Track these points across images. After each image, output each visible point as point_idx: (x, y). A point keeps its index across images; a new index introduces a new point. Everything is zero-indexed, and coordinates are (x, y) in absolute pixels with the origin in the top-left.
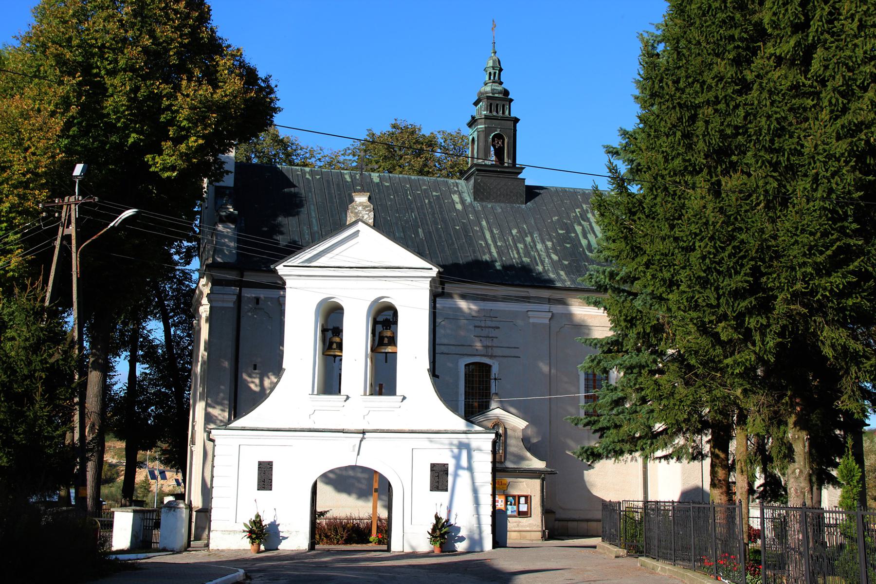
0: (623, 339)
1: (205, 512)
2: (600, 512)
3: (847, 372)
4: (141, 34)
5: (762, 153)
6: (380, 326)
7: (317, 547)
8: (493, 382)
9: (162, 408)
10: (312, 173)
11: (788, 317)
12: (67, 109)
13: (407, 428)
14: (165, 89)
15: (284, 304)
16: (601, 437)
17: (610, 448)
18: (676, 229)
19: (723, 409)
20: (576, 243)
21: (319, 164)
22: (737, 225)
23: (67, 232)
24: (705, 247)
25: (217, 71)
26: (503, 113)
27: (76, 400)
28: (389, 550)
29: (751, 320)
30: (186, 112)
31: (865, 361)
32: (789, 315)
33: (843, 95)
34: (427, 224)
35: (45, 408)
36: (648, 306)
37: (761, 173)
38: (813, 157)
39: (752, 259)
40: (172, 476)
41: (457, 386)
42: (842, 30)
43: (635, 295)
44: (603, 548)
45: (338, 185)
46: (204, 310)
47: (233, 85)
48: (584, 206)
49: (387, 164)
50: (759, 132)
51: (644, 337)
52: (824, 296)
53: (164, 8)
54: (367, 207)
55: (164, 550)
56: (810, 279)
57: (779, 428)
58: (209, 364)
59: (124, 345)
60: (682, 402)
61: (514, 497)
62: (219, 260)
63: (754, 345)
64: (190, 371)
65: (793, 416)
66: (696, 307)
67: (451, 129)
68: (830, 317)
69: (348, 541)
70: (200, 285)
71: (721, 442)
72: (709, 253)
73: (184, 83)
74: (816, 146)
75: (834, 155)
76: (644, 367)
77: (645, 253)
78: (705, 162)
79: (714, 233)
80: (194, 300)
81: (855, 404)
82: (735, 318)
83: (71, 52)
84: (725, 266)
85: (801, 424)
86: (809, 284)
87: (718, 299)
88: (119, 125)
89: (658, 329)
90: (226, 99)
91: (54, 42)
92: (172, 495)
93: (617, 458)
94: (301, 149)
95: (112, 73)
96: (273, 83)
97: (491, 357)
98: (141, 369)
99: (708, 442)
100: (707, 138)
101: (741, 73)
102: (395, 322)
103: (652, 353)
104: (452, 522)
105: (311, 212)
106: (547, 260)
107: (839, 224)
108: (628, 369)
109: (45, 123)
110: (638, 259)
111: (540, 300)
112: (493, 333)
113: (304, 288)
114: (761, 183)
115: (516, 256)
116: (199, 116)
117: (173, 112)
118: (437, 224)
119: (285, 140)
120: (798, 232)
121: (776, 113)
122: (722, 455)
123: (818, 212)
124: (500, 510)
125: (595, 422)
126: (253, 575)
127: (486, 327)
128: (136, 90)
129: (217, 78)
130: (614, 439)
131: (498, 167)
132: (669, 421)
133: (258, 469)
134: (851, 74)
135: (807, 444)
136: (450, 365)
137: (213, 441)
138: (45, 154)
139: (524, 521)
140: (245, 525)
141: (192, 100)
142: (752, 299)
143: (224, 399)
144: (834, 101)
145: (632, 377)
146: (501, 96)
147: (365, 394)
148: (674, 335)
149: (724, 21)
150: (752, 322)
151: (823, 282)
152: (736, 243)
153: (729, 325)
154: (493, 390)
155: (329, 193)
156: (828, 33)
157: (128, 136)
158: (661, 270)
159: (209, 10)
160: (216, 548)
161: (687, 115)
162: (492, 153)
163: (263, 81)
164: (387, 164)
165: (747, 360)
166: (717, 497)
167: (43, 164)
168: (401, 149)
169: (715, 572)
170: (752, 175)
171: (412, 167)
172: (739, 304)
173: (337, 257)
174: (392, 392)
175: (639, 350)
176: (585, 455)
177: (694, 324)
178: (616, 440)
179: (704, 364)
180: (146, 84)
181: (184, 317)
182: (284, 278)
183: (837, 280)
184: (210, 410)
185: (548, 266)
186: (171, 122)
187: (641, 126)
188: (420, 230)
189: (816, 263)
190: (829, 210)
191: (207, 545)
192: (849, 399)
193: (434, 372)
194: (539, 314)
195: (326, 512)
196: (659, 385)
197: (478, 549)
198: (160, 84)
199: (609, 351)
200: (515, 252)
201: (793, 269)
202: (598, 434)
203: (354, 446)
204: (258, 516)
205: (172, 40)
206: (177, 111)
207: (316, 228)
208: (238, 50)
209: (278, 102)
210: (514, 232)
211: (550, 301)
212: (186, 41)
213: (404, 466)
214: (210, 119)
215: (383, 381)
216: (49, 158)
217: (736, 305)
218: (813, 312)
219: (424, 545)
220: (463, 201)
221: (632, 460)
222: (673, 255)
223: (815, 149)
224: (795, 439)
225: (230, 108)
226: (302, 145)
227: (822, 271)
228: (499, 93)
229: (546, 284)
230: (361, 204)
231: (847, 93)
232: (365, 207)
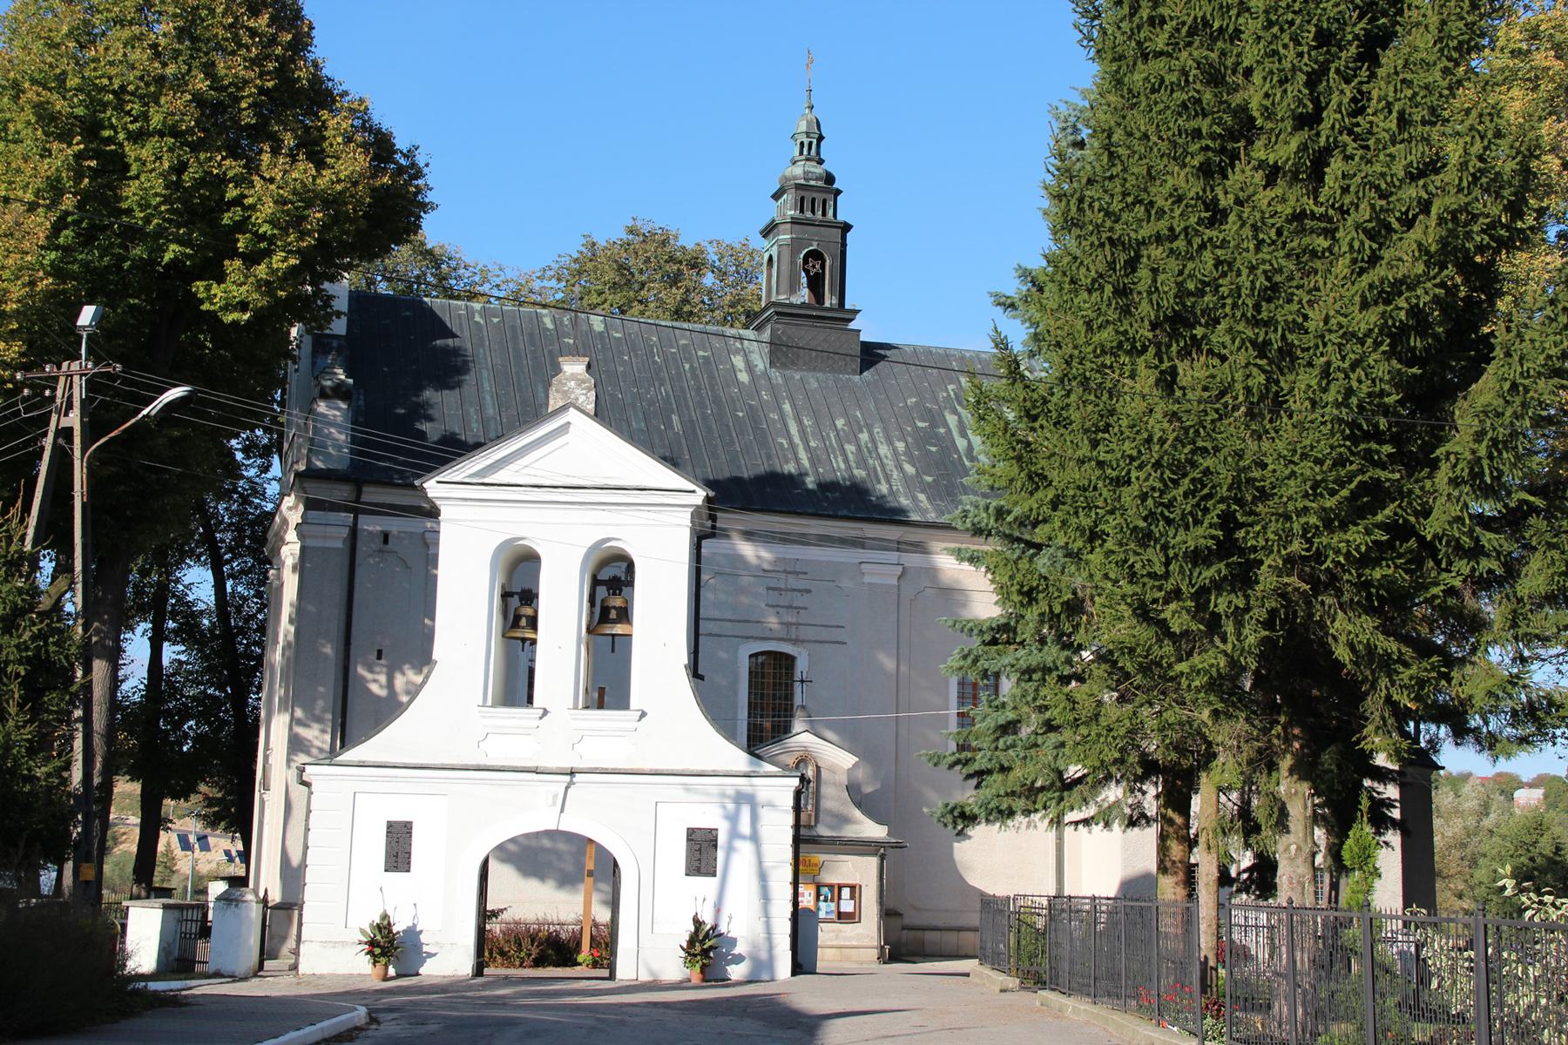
1: (290, 906)
2: (978, 915)
3: (1374, 687)
4: (189, 70)
6: (604, 588)
8: (797, 685)
9: (208, 722)
10: (485, 313)
11: (1280, 595)
12: (55, 203)
13: (647, 766)
14: (231, 168)
15: (437, 544)
16: (978, 786)
18: (1101, 448)
20: (948, 446)
22: (1200, 444)
23: (65, 422)
24: (1147, 479)
25: (324, 138)
26: (824, 214)
27: (78, 713)
28: (612, 977)
30: (268, 208)
31: (1401, 669)
34: (688, 408)
35: (24, 727)
36: (1058, 566)
37: (1241, 358)
38: (1322, 337)
39: (1222, 500)
40: (223, 843)
41: (735, 693)
42: (1370, 132)
45: (531, 335)
46: (290, 551)
47: (351, 163)
49: (618, 298)
51: (1051, 619)
53: (231, 26)
54: (584, 382)
57: (1269, 774)
58: (301, 646)
59: (142, 611)
60: (1111, 730)
61: (831, 887)
62: (319, 464)
63: (1224, 641)
64: (260, 659)
65: (1288, 756)
67: (733, 237)
68: (1346, 597)
69: (539, 962)
70: (284, 507)
71: (1176, 799)
72: (1153, 489)
75: (1354, 335)
76: (1050, 670)
77: (1050, 484)
80: (270, 535)
83: (64, 98)
84: (1178, 511)
85: (1303, 769)
86: (1312, 543)
87: (1167, 564)
89: (1075, 607)
90: (339, 187)
91: (34, 81)
92: (223, 879)
94: (466, 268)
95: (138, 137)
96: (421, 160)
97: (795, 641)
98: (171, 653)
101: (1212, 190)
102: (631, 583)
104: (723, 929)
105: (482, 382)
106: (895, 474)
107: (1363, 446)
108: (1023, 673)
109: (18, 224)
110: (1040, 494)
111: (882, 545)
112: (800, 600)
113: (471, 520)
115: (842, 466)
117: (245, 208)
118: (705, 407)
119: (437, 251)
120: (1296, 459)
121: (1264, 262)
122: (1179, 820)
123: (1329, 426)
124: (807, 910)
125: (967, 762)
126: (381, 1016)
127: (786, 590)
128: (180, 168)
131: (814, 309)
132: (1089, 762)
133: (379, 836)
134: (1384, 202)
136: (722, 655)
137: (307, 784)
138: (18, 278)
139: (848, 929)
140: (363, 932)
142: (1222, 566)
144: (1356, 245)
146: (820, 184)
147: (576, 707)
149: (1184, 105)
150: (1221, 603)
151: (1336, 539)
152: (1196, 474)
154: (798, 700)
155: (515, 350)
156: (1350, 132)
157: (162, 250)
158: (1076, 513)
159: (311, 28)
161: (1123, 257)
162: (804, 280)
163: (405, 156)
164: (618, 298)
165: (1212, 666)
166: (1170, 888)
167: (14, 296)
168: (644, 277)
169: (1159, 1013)
170: (1222, 365)
171: (661, 303)
173: (526, 471)
174: (622, 703)
175: (1043, 641)
176: (949, 818)
179: (1145, 669)
181: (250, 561)
182: (438, 503)
183: (1357, 537)
184: (300, 730)
185: (898, 485)
188: (675, 418)
189: (1324, 509)
190: (1347, 424)
191: (295, 967)
193: (695, 671)
195: (502, 911)
196: (1074, 702)
197: (765, 977)
198: (224, 158)
199: (994, 642)
200: (840, 459)
201: (1288, 518)
202: (974, 782)
204: (385, 916)
205: (246, 82)
206: (253, 207)
207: (490, 411)
208: (362, 101)
211: (900, 546)
212: (270, 84)
213: (641, 834)
215: (607, 687)
216: (24, 285)
218: (1317, 587)
219: (672, 967)
220: (750, 368)
222: (1095, 489)
224: (1290, 796)
226: (468, 260)
228: (817, 179)
229: (892, 516)
230: (574, 377)
231: (1379, 232)
232: (580, 382)
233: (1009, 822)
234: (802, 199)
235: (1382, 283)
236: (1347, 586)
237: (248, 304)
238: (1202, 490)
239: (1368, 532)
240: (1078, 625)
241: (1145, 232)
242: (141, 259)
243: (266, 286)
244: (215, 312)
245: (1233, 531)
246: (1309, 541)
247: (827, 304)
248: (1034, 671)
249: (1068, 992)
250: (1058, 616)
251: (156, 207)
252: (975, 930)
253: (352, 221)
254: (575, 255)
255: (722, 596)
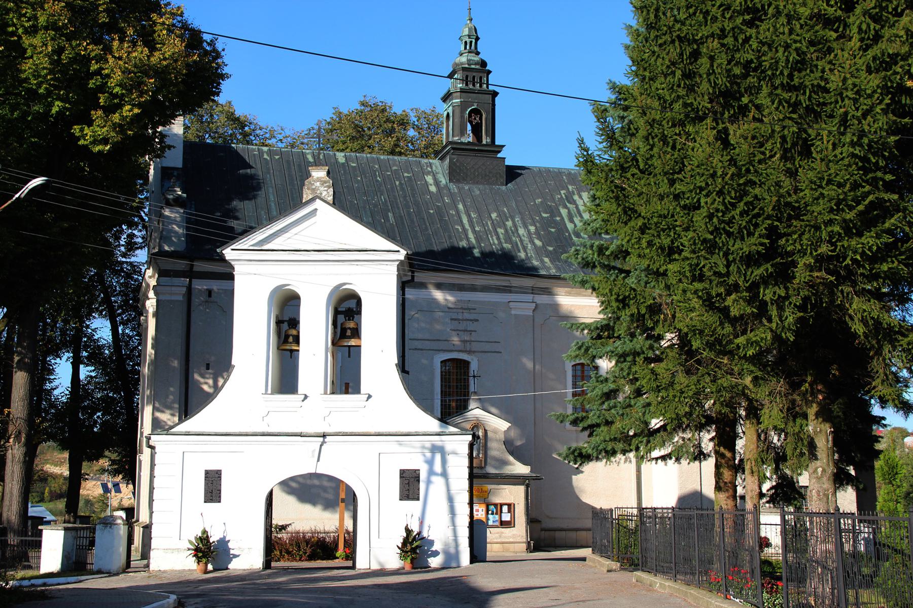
0: (615, 323)
5: (779, 91)
7: (273, 564)
8: (471, 378)
10: (270, 153)
13: (372, 431)
14: (93, 50)
16: (590, 435)
17: (600, 448)
19: (730, 401)
20: (562, 227)
21: (280, 145)
22: (750, 177)
24: (713, 203)
25: (155, 32)
26: (481, 86)
28: (353, 567)
29: (767, 291)
30: (118, 76)
31: (901, 338)
32: (811, 285)
33: (876, 19)
34: (398, 208)
36: (643, 284)
38: (841, 94)
39: (769, 217)
40: (126, 489)
41: (432, 384)
43: (628, 273)
44: (594, 561)
45: (299, 166)
46: (151, 304)
47: (172, 47)
48: (570, 187)
49: (356, 145)
50: (775, 65)
52: (854, 261)
54: (325, 182)
55: (99, 572)
56: (838, 240)
60: (682, 392)
61: (496, 505)
62: (167, 248)
63: (770, 320)
65: (814, 405)
66: (701, 278)
67: (425, 107)
69: (312, 558)
70: (146, 276)
71: (726, 440)
72: (717, 210)
73: (116, 44)
74: (845, 80)
76: (639, 354)
77: (640, 215)
78: (709, 106)
79: (724, 187)
80: (141, 294)
81: (890, 390)
82: (748, 289)
84: (736, 226)
85: (824, 414)
87: (728, 266)
88: (41, 91)
90: (165, 63)
93: (608, 459)
94: (261, 129)
95: (33, 31)
96: (219, 46)
97: (470, 352)
99: (711, 440)
100: (712, 78)
102: (359, 312)
103: (647, 338)
104: (425, 534)
105: (269, 194)
106: (529, 246)
107: (870, 175)
110: (632, 223)
111: (522, 290)
112: (471, 326)
113: (255, 273)
114: (777, 128)
115: (496, 242)
116: (133, 85)
118: (409, 208)
119: (242, 119)
121: (795, 42)
122: (728, 454)
124: (480, 521)
125: (583, 419)
127: (463, 320)
128: (60, 51)
129: (154, 40)
130: (605, 437)
132: (668, 415)
133: (208, 479)
135: (830, 438)
136: (425, 362)
137: (152, 448)
139: (507, 531)
140: (190, 542)
141: (125, 63)
142: (769, 266)
143: (173, 402)
144: (864, 27)
145: (625, 365)
146: (478, 67)
147: (325, 393)
148: (674, 317)
150: (767, 294)
152: (749, 199)
153: (741, 298)
154: (472, 389)
157: (51, 105)
158: (659, 236)
160: (157, 569)
161: (688, 50)
162: (469, 127)
163: (209, 44)
165: (762, 339)
166: (722, 501)
169: (725, 589)
170: (771, 113)
172: (752, 272)
176: (572, 457)
177: (699, 297)
178: (607, 439)
179: (710, 346)
180: (71, 45)
182: (233, 263)
183: (869, 240)
184: (158, 414)
185: (531, 253)
186: (102, 88)
187: (634, 68)
188: (390, 215)
189: (844, 221)
192: (882, 384)
193: (403, 367)
194: (522, 305)
195: (288, 525)
196: (656, 375)
197: (454, 565)
198: (88, 44)
199: (599, 337)
201: (817, 228)
202: (587, 433)
203: (314, 451)
204: (205, 532)
206: (108, 76)
208: (179, 8)
209: (225, 68)
210: (494, 215)
211: (534, 291)
213: (371, 473)
214: (146, 85)
215: (346, 379)
217: (749, 273)
218: (841, 280)
219: (393, 561)
220: (437, 183)
221: (625, 462)
223: (844, 84)
225: (170, 74)
226: (262, 124)
227: (849, 230)
228: (476, 64)
229: (529, 271)
230: (319, 179)
232: (323, 183)
233: (612, 459)
234: (467, 77)
235: (883, 55)
236: (860, 279)
237: (108, 139)
238: (753, 212)
239: (878, 236)
240: (658, 321)
241: (705, 31)
242: (38, 112)
243: (120, 128)
244: (87, 145)
245: (776, 241)
246: (834, 244)
247: (484, 142)
248: (628, 355)
249: (657, 570)
250: (644, 315)
251: (45, 77)
252: (589, 530)
253: (175, 85)
254: (329, 120)
255: (423, 325)
